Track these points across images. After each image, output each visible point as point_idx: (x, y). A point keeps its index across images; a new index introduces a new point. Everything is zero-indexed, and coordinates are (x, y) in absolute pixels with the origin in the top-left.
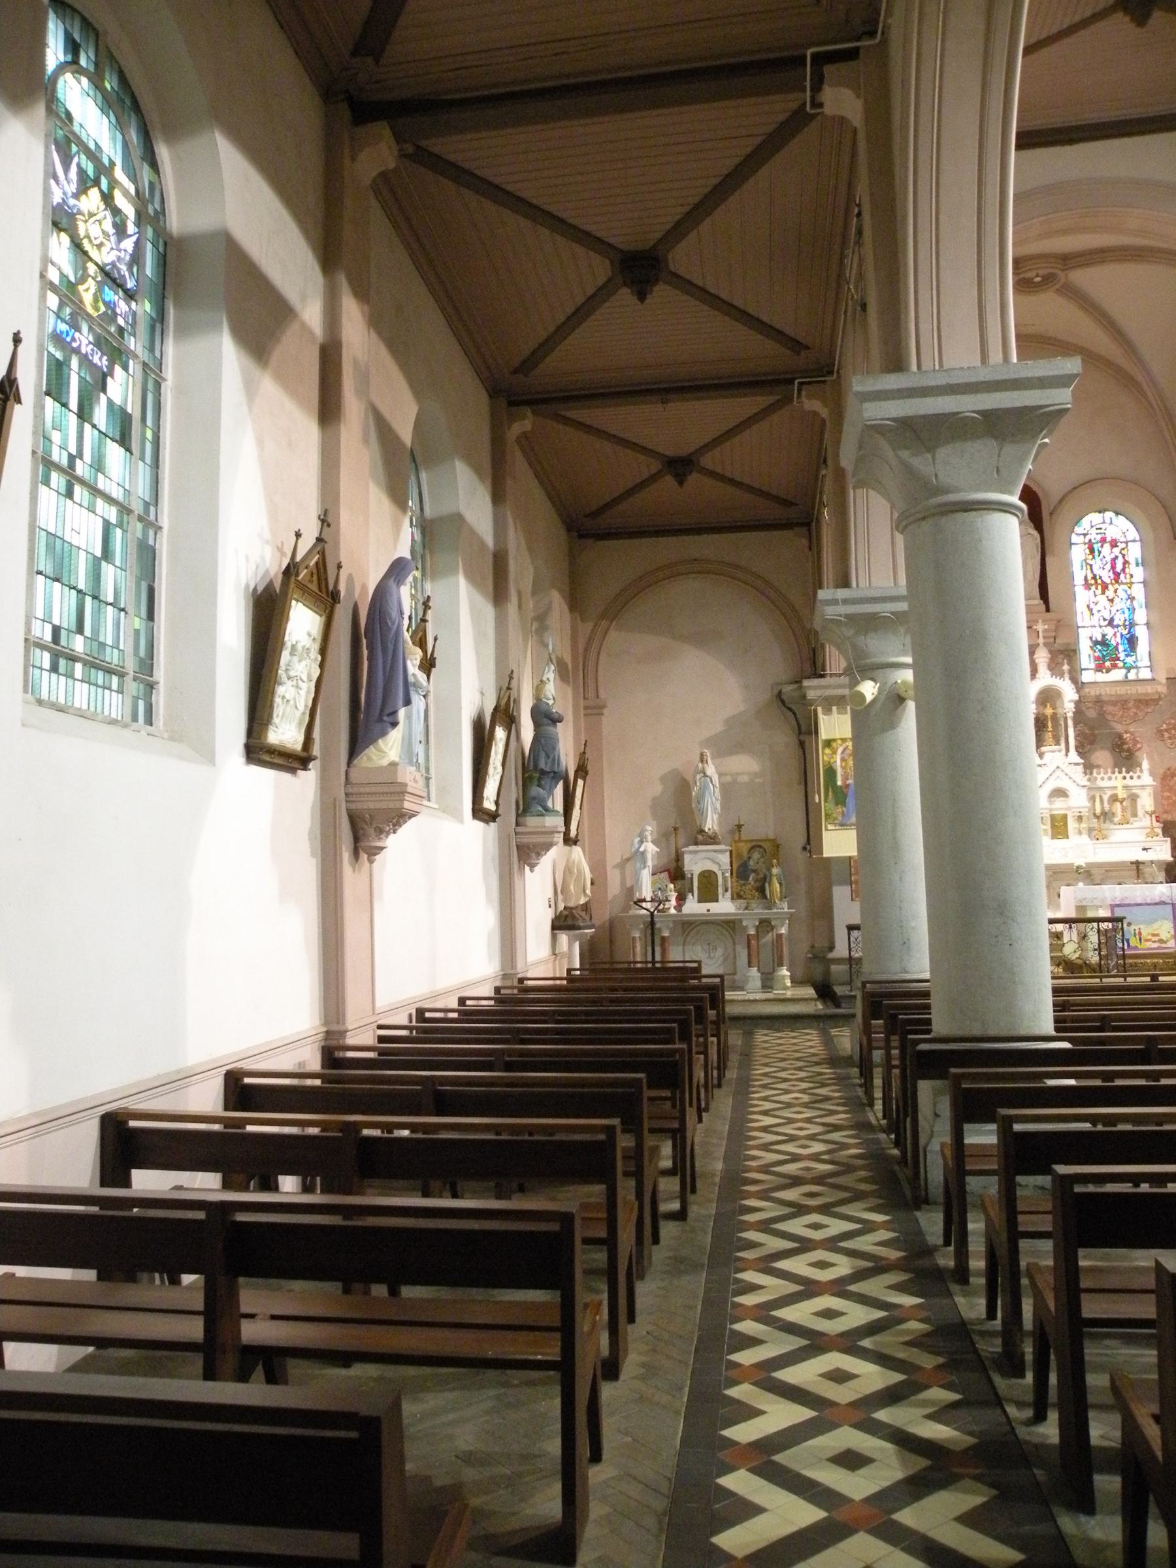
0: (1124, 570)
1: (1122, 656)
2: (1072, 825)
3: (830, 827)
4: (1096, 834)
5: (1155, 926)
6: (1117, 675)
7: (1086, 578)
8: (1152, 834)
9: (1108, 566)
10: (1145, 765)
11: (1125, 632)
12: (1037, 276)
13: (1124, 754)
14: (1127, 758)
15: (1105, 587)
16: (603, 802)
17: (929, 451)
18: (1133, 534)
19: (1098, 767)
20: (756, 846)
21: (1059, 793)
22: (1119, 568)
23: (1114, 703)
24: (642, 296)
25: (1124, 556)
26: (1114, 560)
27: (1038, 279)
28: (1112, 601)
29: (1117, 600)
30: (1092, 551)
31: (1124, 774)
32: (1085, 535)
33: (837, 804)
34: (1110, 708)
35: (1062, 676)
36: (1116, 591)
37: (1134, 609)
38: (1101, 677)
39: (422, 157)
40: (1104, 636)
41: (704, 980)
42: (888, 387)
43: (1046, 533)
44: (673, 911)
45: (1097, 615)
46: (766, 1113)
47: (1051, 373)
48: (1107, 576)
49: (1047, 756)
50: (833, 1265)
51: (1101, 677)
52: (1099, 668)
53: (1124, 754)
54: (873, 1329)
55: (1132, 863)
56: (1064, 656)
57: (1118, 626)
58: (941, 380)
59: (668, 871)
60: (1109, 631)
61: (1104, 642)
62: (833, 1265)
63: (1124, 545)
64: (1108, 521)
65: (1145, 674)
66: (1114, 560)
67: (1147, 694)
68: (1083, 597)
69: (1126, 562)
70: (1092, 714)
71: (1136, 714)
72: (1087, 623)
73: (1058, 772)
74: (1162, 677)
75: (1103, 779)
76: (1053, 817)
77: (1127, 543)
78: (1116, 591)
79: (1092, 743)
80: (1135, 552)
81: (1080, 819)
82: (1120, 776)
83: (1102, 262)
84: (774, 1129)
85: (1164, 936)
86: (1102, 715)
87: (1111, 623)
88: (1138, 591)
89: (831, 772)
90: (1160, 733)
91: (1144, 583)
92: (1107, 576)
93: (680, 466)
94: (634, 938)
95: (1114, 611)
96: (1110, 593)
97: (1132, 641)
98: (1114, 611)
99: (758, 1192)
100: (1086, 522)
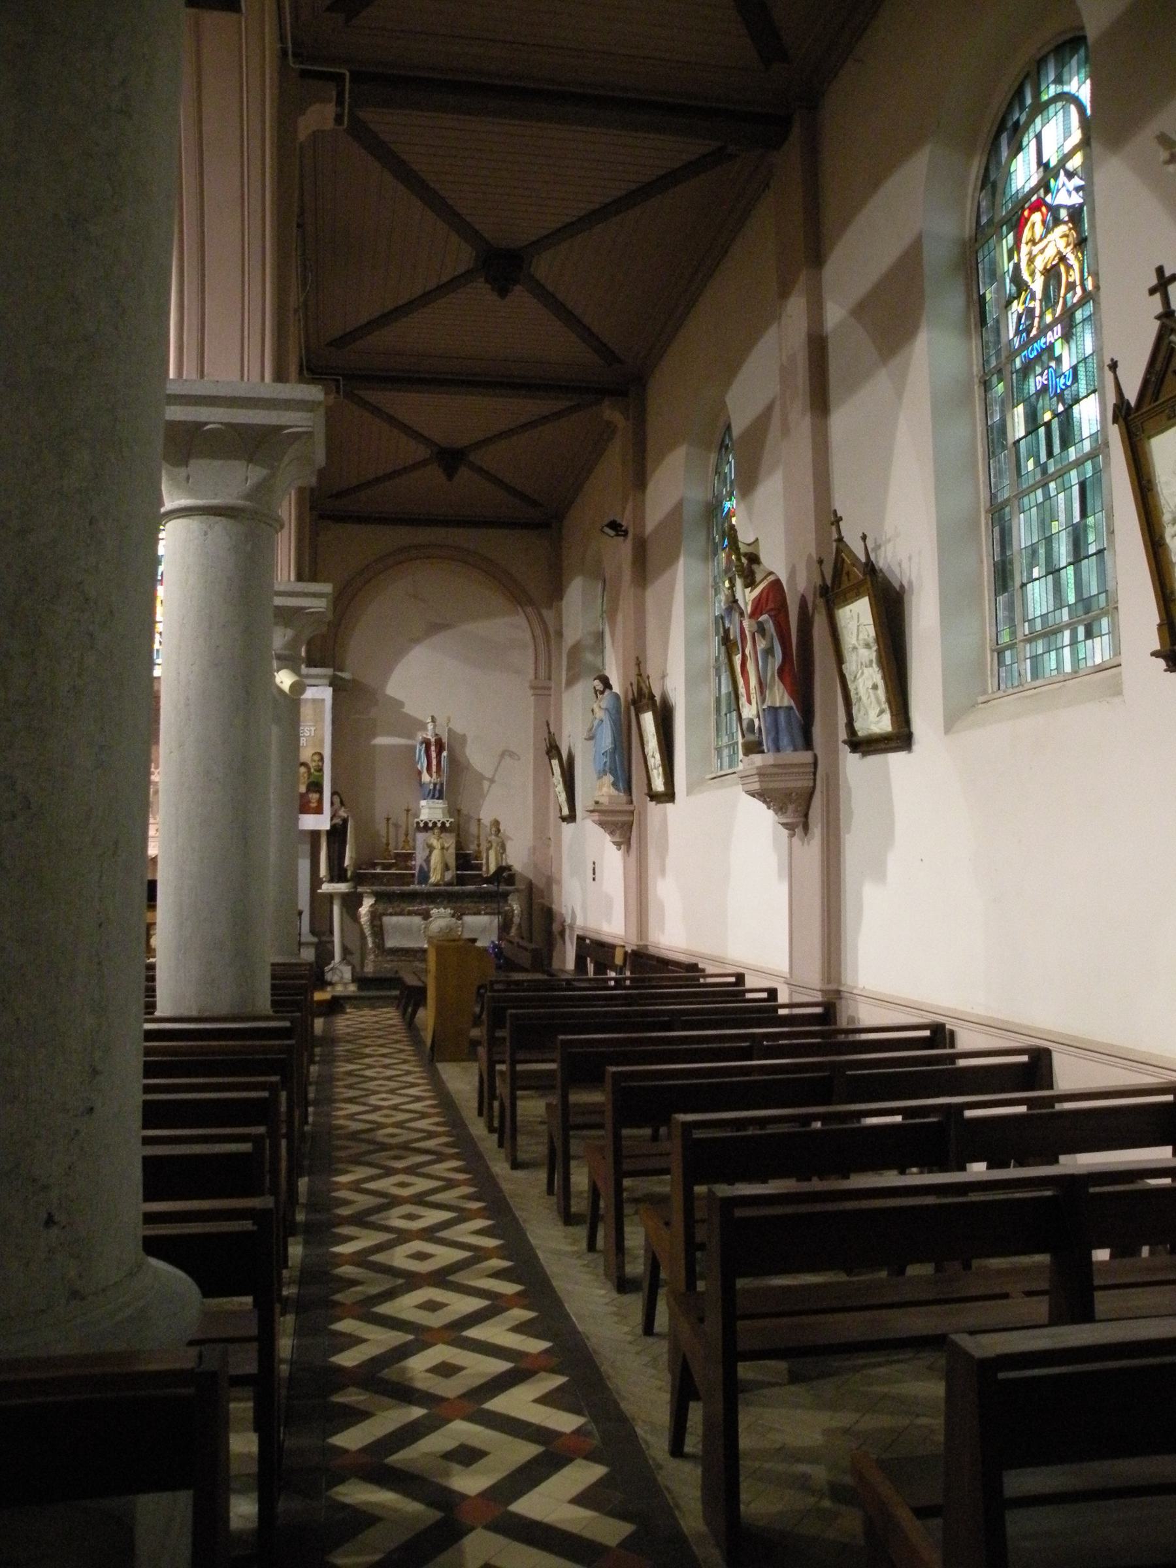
24: (503, 292)
39: (359, 131)
46: (351, 1100)
50: (409, 1256)
54: (390, 1295)
62: (409, 1256)
84: (360, 1117)
93: (451, 459)
99: (487, 1259)
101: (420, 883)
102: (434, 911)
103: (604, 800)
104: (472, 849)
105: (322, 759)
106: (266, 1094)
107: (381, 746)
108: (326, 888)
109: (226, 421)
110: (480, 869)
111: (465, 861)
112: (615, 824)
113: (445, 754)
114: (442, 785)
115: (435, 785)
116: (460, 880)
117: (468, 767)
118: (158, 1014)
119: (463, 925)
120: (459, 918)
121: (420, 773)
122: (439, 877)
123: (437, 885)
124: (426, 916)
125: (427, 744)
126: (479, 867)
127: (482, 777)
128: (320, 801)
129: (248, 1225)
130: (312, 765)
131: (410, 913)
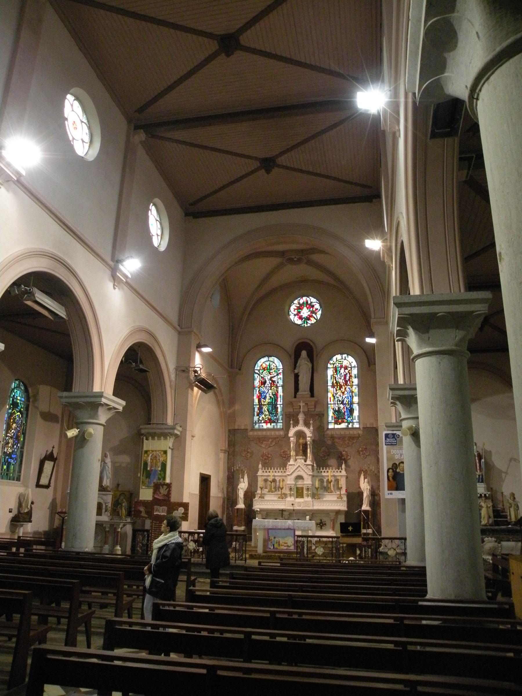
0: (349, 379)
1: (346, 417)
2: (305, 492)
3: (143, 487)
5: (286, 539)
6: (343, 425)
7: (333, 383)
8: (340, 497)
9: (343, 378)
11: (348, 407)
12: (295, 258)
15: (341, 387)
18: (354, 364)
19: (331, 466)
20: (123, 493)
21: (300, 477)
22: (348, 378)
23: (339, 438)
25: (350, 373)
27: (296, 259)
28: (343, 393)
29: (346, 393)
30: (336, 371)
31: (276, 470)
32: (333, 364)
33: (147, 478)
34: (337, 440)
36: (345, 389)
37: (353, 397)
38: (337, 426)
40: (339, 408)
41: (34, 551)
43: (315, 363)
45: (336, 399)
48: (342, 381)
51: (337, 426)
52: (336, 423)
55: (280, 510)
57: (345, 404)
60: (342, 406)
63: (349, 369)
64: (344, 358)
65: (356, 425)
67: (354, 434)
69: (350, 376)
71: (348, 443)
72: (332, 402)
73: (299, 469)
75: (324, 472)
76: (297, 488)
77: (351, 368)
78: (345, 389)
79: (328, 455)
80: (355, 372)
81: (308, 489)
86: (333, 443)
88: (355, 389)
89: (146, 464)
90: (359, 452)
91: (358, 385)
92: (342, 381)
95: (344, 397)
96: (343, 390)
97: (351, 411)
98: (344, 397)
100: (334, 358)
102: (486, 539)
104: (500, 507)
106: (84, 589)
109: (447, 311)
110: (507, 518)
111: (498, 514)
113: (483, 460)
114: (482, 476)
115: (479, 476)
116: (496, 523)
117: (494, 466)
118: (428, 597)
119: (501, 547)
120: (500, 543)
122: (486, 522)
123: (485, 525)
126: (506, 517)
127: (501, 472)
129: (204, 671)
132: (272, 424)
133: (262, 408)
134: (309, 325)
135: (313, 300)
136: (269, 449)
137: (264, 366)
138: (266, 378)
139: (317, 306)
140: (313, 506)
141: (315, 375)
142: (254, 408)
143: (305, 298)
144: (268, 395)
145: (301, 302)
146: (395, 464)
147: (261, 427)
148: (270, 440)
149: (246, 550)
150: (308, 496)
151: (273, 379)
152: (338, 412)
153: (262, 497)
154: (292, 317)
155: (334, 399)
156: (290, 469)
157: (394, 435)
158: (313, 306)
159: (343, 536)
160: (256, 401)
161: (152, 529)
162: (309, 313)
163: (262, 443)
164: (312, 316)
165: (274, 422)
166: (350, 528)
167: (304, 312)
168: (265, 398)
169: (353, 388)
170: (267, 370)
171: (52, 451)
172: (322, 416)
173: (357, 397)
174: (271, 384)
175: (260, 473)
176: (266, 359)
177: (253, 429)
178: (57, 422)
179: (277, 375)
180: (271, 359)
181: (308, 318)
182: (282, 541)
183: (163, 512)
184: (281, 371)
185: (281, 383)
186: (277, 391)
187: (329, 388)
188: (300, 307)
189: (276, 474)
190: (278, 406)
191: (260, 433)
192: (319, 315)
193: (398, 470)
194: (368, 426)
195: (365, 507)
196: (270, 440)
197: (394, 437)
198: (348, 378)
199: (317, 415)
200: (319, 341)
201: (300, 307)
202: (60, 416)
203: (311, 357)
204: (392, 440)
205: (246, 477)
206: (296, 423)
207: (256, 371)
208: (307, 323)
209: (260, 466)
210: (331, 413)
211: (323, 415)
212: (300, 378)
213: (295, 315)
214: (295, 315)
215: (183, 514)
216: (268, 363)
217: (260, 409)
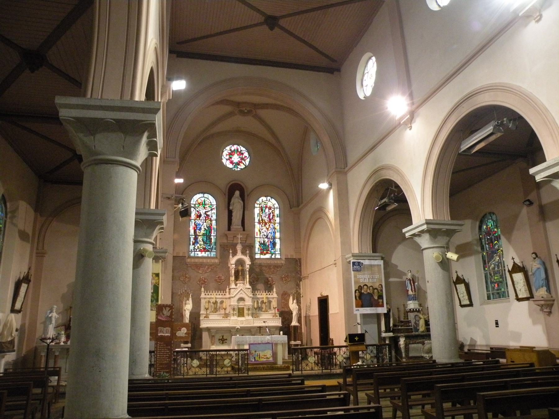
0: (273, 218)
1: (270, 249)
2: (246, 312)
4: (253, 315)
5: (265, 352)
6: (268, 256)
8: (275, 315)
9: (267, 216)
10: (274, 290)
13: (269, 286)
14: (269, 287)
15: (266, 224)
16: (39, 295)
17: (92, 135)
18: (277, 205)
21: (241, 299)
22: (271, 217)
23: (266, 267)
26: (269, 214)
28: (268, 229)
30: (262, 210)
32: (260, 204)
34: (264, 268)
35: (246, 255)
38: (262, 257)
40: (264, 241)
42: (72, 103)
44: (62, 344)
45: (262, 234)
47: (147, 107)
48: (266, 219)
49: (238, 285)
51: (262, 257)
52: (262, 253)
53: (269, 286)
55: (258, 327)
56: (249, 248)
57: (269, 238)
58: (98, 103)
59: (65, 326)
60: (266, 240)
61: (264, 244)
65: (278, 256)
66: (269, 214)
68: (257, 227)
69: (273, 216)
70: (257, 270)
72: (258, 236)
73: (241, 292)
74: (284, 258)
76: (239, 309)
77: (274, 208)
79: (257, 281)
80: (277, 212)
81: (249, 309)
82: (215, 294)
83: (267, 108)
85: (269, 356)
86: (261, 270)
87: (267, 237)
88: (277, 227)
90: (282, 278)
92: (266, 219)
94: (42, 356)
97: (274, 244)
100: (260, 199)
101: (415, 332)
102: (426, 342)
103: (545, 296)
105: (382, 287)
107: (392, 282)
108: (384, 335)
112: (548, 305)
121: (408, 291)
123: (423, 332)
124: (423, 344)
125: (410, 280)
128: (383, 302)
130: (379, 289)
131: (418, 343)
132: (207, 253)
133: (197, 238)
134: (239, 169)
135: (243, 149)
136: (206, 275)
137: (200, 201)
138: (201, 212)
139: (246, 154)
140: (254, 323)
141: (246, 212)
142: (190, 238)
143: (235, 146)
144: (202, 227)
145: (233, 149)
146: (360, 286)
147: (196, 255)
148: (207, 267)
149: (54, 368)
150: (248, 315)
151: (208, 213)
152: (263, 244)
153: (207, 317)
154: (224, 161)
155: (260, 233)
156: (233, 293)
157: (359, 263)
158: (243, 154)
159: (351, 345)
160: (192, 232)
161: (157, 350)
162: (239, 159)
163: (199, 269)
164: (241, 162)
165: (208, 251)
166: (357, 338)
167: (234, 157)
168: (200, 229)
169: (276, 224)
170: (202, 204)
171: (514, 262)
172: (251, 247)
173: (279, 233)
174: (206, 217)
175: (203, 295)
176: (201, 195)
177: (190, 257)
178: (28, 241)
179: (212, 210)
180: (206, 195)
181: (238, 164)
182: (262, 354)
183: (166, 333)
184: (215, 207)
185: (214, 217)
186: (211, 224)
187: (256, 224)
188: (231, 154)
189: (218, 296)
190: (212, 237)
191: (197, 260)
192: (247, 162)
193: (363, 291)
194: (289, 257)
195: (294, 323)
196: (207, 267)
197: (359, 265)
198: (271, 217)
199: (248, 246)
200: (249, 184)
201: (231, 154)
202: (31, 234)
203: (242, 196)
204: (358, 267)
205: (190, 299)
206: (235, 254)
207: (193, 205)
208: (237, 168)
209: (203, 289)
210: (257, 246)
211: (253, 246)
212: (234, 214)
213: (227, 160)
214: (227, 160)
215: (185, 334)
216: (203, 199)
217: (196, 239)
